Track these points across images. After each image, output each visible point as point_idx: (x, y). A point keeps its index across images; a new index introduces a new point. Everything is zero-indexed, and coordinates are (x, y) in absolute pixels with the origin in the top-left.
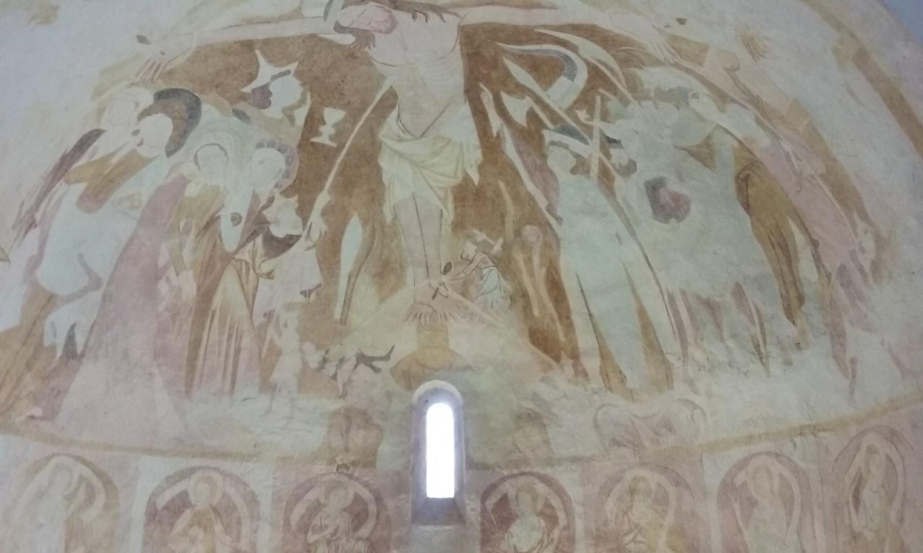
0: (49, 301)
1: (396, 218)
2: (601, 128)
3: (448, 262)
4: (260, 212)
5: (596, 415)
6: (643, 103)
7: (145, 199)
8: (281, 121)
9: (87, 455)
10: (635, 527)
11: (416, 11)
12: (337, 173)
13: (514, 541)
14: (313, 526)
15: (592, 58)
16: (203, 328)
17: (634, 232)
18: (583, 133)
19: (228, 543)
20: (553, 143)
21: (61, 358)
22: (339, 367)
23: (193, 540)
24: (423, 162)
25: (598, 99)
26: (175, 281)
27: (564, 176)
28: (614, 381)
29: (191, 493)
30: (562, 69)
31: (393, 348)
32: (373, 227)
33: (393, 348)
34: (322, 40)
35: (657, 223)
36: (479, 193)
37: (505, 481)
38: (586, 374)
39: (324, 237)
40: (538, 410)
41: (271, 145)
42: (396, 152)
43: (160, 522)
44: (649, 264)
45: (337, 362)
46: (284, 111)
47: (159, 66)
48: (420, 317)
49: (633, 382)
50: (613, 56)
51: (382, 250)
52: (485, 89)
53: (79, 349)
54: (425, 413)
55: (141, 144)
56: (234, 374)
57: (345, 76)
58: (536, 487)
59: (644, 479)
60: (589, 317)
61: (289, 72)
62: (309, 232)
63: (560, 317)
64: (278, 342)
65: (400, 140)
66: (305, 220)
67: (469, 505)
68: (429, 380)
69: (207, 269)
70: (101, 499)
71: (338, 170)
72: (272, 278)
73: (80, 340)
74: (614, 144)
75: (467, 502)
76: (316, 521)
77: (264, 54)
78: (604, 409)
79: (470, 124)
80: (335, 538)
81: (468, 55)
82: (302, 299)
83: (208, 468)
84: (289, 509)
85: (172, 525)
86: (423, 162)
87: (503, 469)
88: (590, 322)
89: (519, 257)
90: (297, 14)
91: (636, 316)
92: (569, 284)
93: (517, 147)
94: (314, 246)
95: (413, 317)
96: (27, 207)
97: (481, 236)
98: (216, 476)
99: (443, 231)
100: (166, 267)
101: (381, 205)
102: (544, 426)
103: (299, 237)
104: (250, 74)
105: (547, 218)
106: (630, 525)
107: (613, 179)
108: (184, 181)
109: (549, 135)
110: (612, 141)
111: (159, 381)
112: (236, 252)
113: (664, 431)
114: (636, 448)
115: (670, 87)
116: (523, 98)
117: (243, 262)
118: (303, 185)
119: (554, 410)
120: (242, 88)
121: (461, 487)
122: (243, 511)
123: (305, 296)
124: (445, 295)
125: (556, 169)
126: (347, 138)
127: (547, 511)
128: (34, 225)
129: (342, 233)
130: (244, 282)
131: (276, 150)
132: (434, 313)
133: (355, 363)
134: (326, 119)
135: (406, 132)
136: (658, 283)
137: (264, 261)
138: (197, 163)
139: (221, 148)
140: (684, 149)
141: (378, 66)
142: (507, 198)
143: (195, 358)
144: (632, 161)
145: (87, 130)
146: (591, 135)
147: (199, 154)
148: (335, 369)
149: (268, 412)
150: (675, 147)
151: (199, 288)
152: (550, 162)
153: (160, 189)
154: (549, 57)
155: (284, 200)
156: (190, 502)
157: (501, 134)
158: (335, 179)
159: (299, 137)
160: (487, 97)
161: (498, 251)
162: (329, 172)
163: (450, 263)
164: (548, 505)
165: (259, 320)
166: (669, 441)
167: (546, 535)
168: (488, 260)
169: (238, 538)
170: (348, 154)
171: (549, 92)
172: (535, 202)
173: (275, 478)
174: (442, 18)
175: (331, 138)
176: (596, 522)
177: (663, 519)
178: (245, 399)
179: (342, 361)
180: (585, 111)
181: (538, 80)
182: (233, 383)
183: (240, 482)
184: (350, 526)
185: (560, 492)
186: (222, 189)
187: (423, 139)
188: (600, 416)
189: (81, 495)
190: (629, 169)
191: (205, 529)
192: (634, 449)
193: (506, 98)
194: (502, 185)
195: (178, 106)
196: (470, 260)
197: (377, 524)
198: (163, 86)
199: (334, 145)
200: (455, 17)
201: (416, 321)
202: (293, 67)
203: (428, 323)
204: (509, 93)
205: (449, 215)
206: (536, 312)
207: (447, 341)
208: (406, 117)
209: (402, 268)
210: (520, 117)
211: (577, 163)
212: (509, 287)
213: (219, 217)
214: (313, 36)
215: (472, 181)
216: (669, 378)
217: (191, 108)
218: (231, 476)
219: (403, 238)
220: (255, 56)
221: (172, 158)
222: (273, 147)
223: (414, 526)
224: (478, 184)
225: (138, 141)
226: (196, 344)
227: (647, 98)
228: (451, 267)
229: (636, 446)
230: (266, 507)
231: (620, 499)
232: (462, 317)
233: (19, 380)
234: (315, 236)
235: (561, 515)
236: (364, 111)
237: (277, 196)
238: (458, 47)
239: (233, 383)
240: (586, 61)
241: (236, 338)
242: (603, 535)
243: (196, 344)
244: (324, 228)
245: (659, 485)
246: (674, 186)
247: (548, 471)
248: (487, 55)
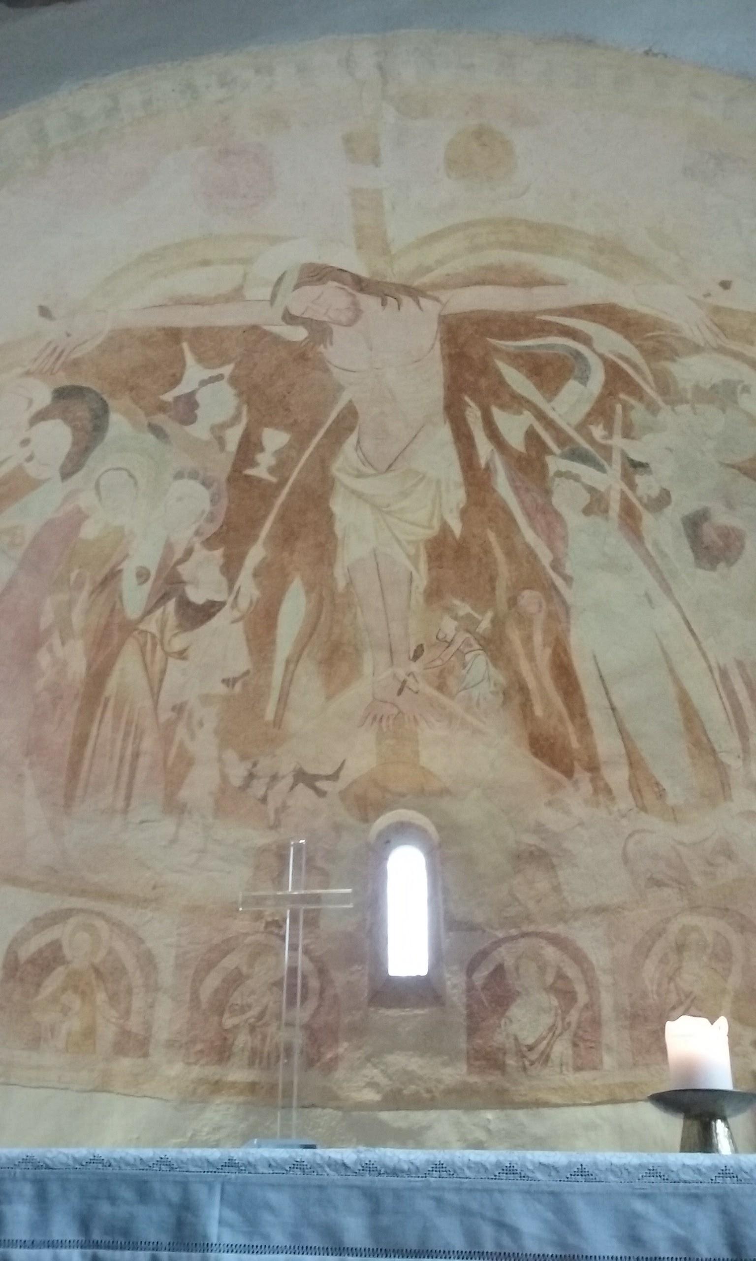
1: (350, 583)
2: (624, 448)
3: (420, 643)
5: (624, 848)
6: (680, 408)
7: (29, 535)
10: (687, 996)
11: (386, 295)
13: (514, 1028)
14: (231, 1006)
15: (610, 351)
17: (670, 590)
18: (598, 457)
19: (114, 1020)
20: (559, 474)
22: (269, 787)
23: (66, 1011)
24: (388, 506)
25: (619, 408)
26: (60, 651)
27: (573, 519)
28: (649, 797)
29: (65, 943)
30: (571, 371)
31: (343, 764)
32: (321, 595)
33: (343, 764)
34: (266, 333)
35: (700, 572)
36: (461, 550)
37: (500, 946)
38: (608, 791)
40: (543, 846)
41: (194, 475)
42: (353, 492)
43: (22, 980)
44: (691, 630)
46: (213, 429)
47: (63, 351)
49: (675, 795)
50: (637, 347)
52: (472, 404)
54: (387, 859)
55: (30, 459)
57: (292, 385)
58: (543, 952)
59: (695, 929)
60: (610, 712)
61: (220, 377)
62: (236, 597)
63: (572, 716)
65: (360, 475)
67: (449, 979)
68: (392, 810)
74: (641, 469)
75: (447, 975)
76: (237, 998)
77: (193, 349)
78: (637, 837)
79: (451, 453)
80: (260, 1023)
81: (450, 356)
82: (222, 689)
83: (91, 912)
84: (198, 979)
85: (39, 985)
86: (388, 506)
87: (497, 929)
88: (613, 720)
89: (515, 635)
90: (236, 295)
91: (677, 705)
92: (583, 668)
93: (512, 481)
95: (371, 721)
97: (464, 609)
98: (100, 923)
99: (413, 602)
101: (331, 565)
102: (553, 867)
103: (222, 604)
104: (174, 375)
105: (551, 579)
106: (678, 994)
107: (640, 519)
108: (78, 518)
109: (555, 463)
110: (637, 466)
111: (30, 788)
112: (142, 619)
113: (721, 859)
114: (683, 887)
115: (713, 382)
116: (521, 413)
119: (567, 845)
121: (438, 958)
122: (137, 979)
124: (415, 689)
125: (563, 510)
126: (291, 470)
127: (560, 984)
129: (280, 602)
132: (400, 715)
135: (367, 464)
136: (704, 655)
137: (176, 635)
138: (98, 493)
139: (131, 476)
140: (733, 466)
141: (335, 371)
142: (498, 553)
144: (665, 490)
146: (609, 459)
148: (264, 789)
149: (174, 841)
150: (722, 464)
151: (89, 667)
152: (556, 500)
153: (49, 525)
154: (555, 354)
155: (205, 552)
156: (64, 957)
157: (492, 466)
158: (272, 527)
160: (473, 415)
161: (486, 628)
162: (265, 517)
163: (421, 646)
164: (561, 976)
166: (729, 872)
167: (559, 1018)
168: (473, 641)
169: (128, 1012)
170: (291, 493)
171: (553, 404)
172: (536, 557)
173: (180, 935)
174: (418, 303)
175: (272, 470)
176: (630, 995)
177: (726, 981)
178: (142, 822)
179: (274, 778)
180: (601, 426)
181: (540, 386)
182: (128, 798)
183: (131, 935)
185: (579, 958)
187: (390, 475)
188: (631, 846)
190: (662, 500)
191: (83, 994)
192: (680, 889)
193: (497, 414)
194: (492, 537)
195: (82, 411)
197: (320, 1006)
198: (64, 380)
199: (273, 480)
200: (436, 303)
201: (376, 725)
202: (227, 370)
204: (502, 407)
205: (422, 580)
206: (539, 711)
207: (417, 753)
208: (367, 445)
209: (358, 653)
210: (516, 439)
211: (591, 499)
212: (501, 678)
213: (120, 571)
214: (255, 327)
215: (452, 532)
216: (725, 786)
217: (96, 417)
219: (359, 609)
220: (182, 351)
223: (372, 1009)
224: (461, 536)
225: (28, 454)
226: (81, 741)
227: (682, 401)
229: (683, 884)
230: (166, 975)
231: (664, 960)
232: (438, 721)
234: (244, 604)
235: (581, 990)
236: (313, 434)
237: (198, 546)
238: (438, 345)
239: (128, 798)
240: (601, 356)
241: (135, 738)
242: (640, 1012)
243: (81, 741)
244: (256, 593)
245: (718, 934)
246: (722, 517)
247: (560, 929)
248: (475, 357)
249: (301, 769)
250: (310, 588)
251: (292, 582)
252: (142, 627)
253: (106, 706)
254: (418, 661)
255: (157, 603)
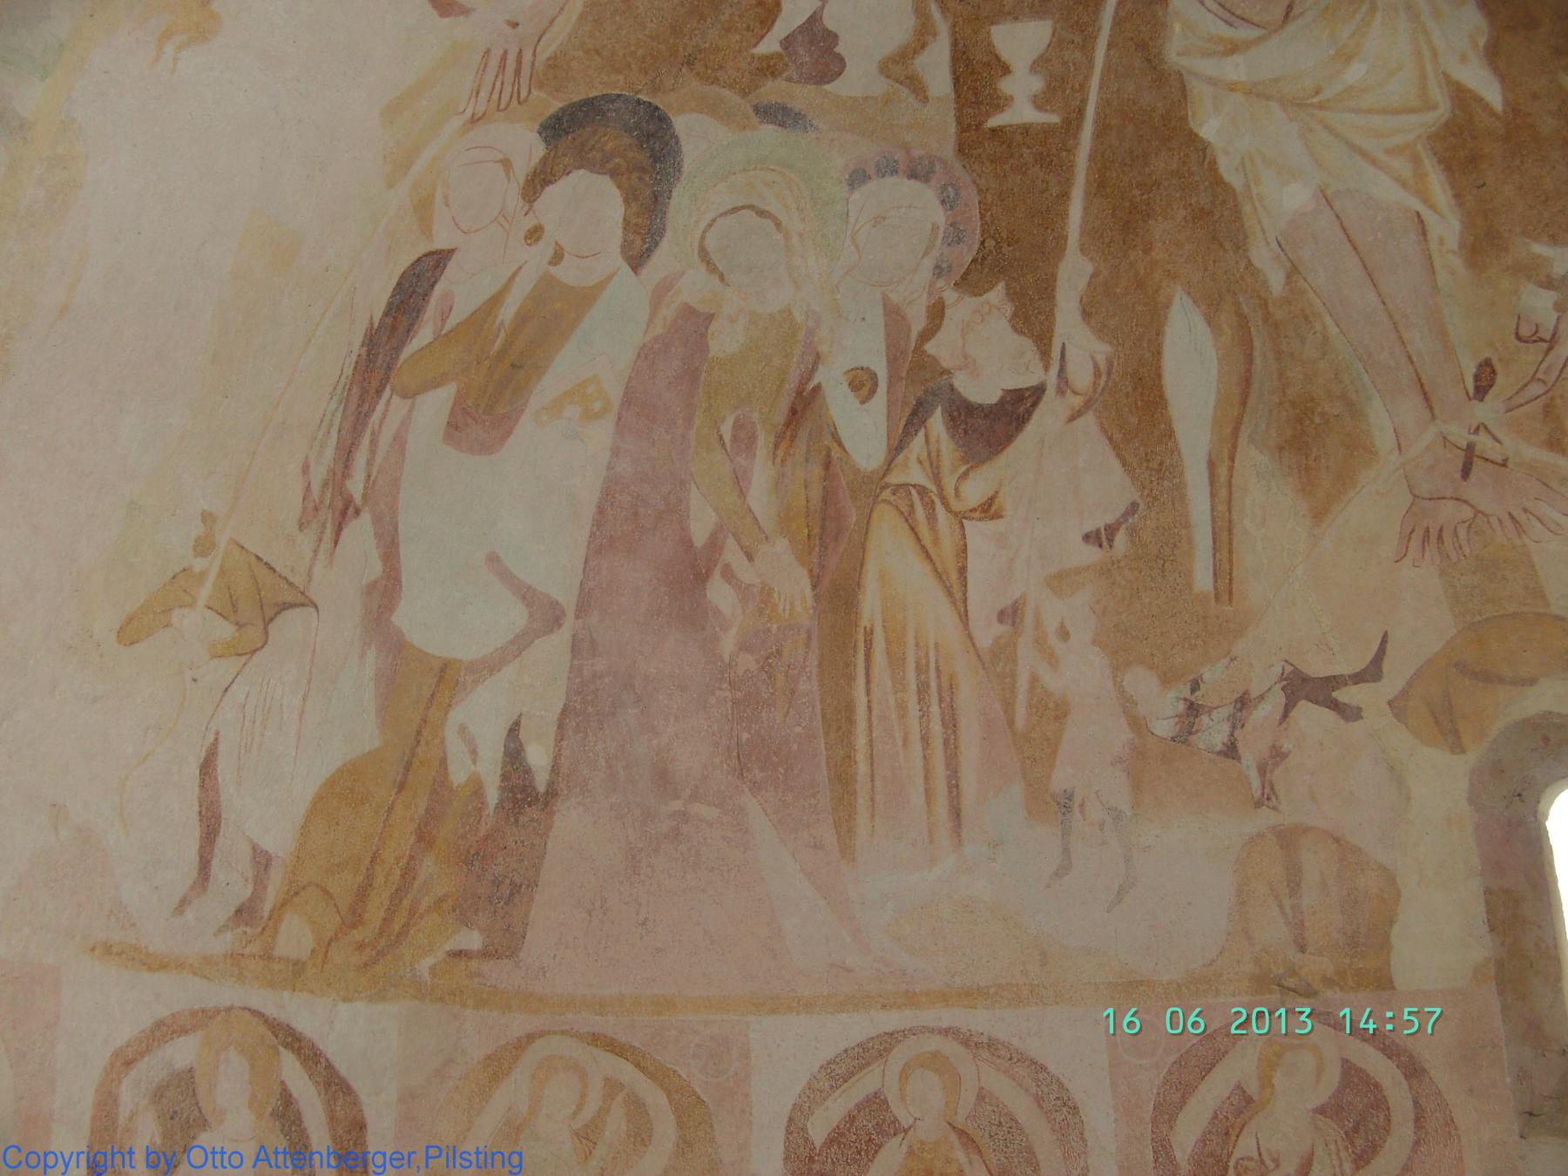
0: (441, 679)
1: (1293, 271)
4: (918, 350)
8: (887, 100)
9: (608, 1024)
12: (1087, 193)
16: (850, 678)
21: (500, 806)
22: (1236, 723)
26: (746, 573)
29: (891, 1095)
32: (1239, 313)
39: (1109, 373)
41: (888, 168)
45: (1229, 710)
48: (1440, 537)
51: (1281, 374)
53: (541, 781)
55: (557, 257)
56: (954, 787)
62: (1062, 369)
64: (1050, 680)
65: (1234, 48)
66: (1043, 341)
69: (823, 528)
70: (666, 1128)
71: (1087, 181)
72: (998, 516)
73: (538, 757)
82: (1091, 554)
94: (1087, 405)
96: (319, 474)
99: (1442, 277)
100: (715, 545)
101: (1240, 246)
103: (1038, 391)
117: (913, 492)
118: (1006, 249)
120: (756, 45)
123: (1100, 546)
126: (1083, 87)
128: (351, 511)
130: (929, 547)
131: (905, 180)
133: (1284, 700)
134: (1005, 55)
135: (1237, 22)
137: (965, 475)
138: (711, 267)
139: (762, 213)
143: (849, 758)
145: (405, 261)
147: (711, 244)
148: (1226, 728)
155: (971, 302)
159: (952, 129)
162: (1065, 196)
165: (987, 633)
170: (1102, 131)
175: (1039, 103)
179: (1243, 702)
184: (1343, 1154)
186: (799, 317)
187: (1291, 27)
189: (616, 1125)
196: (1548, 337)
199: (1054, 119)
203: (1467, 551)
205: (1447, 227)
218: (992, 1045)
221: (644, 271)
222: (894, 172)
224: (1506, 102)
225: (550, 253)
228: (1494, 372)
233: (408, 874)
234: (1081, 376)
249: (1296, 672)
250: (1211, 306)
251: (1167, 306)
252: (894, 478)
253: (869, 644)
254: (1489, 397)
255: (909, 423)
